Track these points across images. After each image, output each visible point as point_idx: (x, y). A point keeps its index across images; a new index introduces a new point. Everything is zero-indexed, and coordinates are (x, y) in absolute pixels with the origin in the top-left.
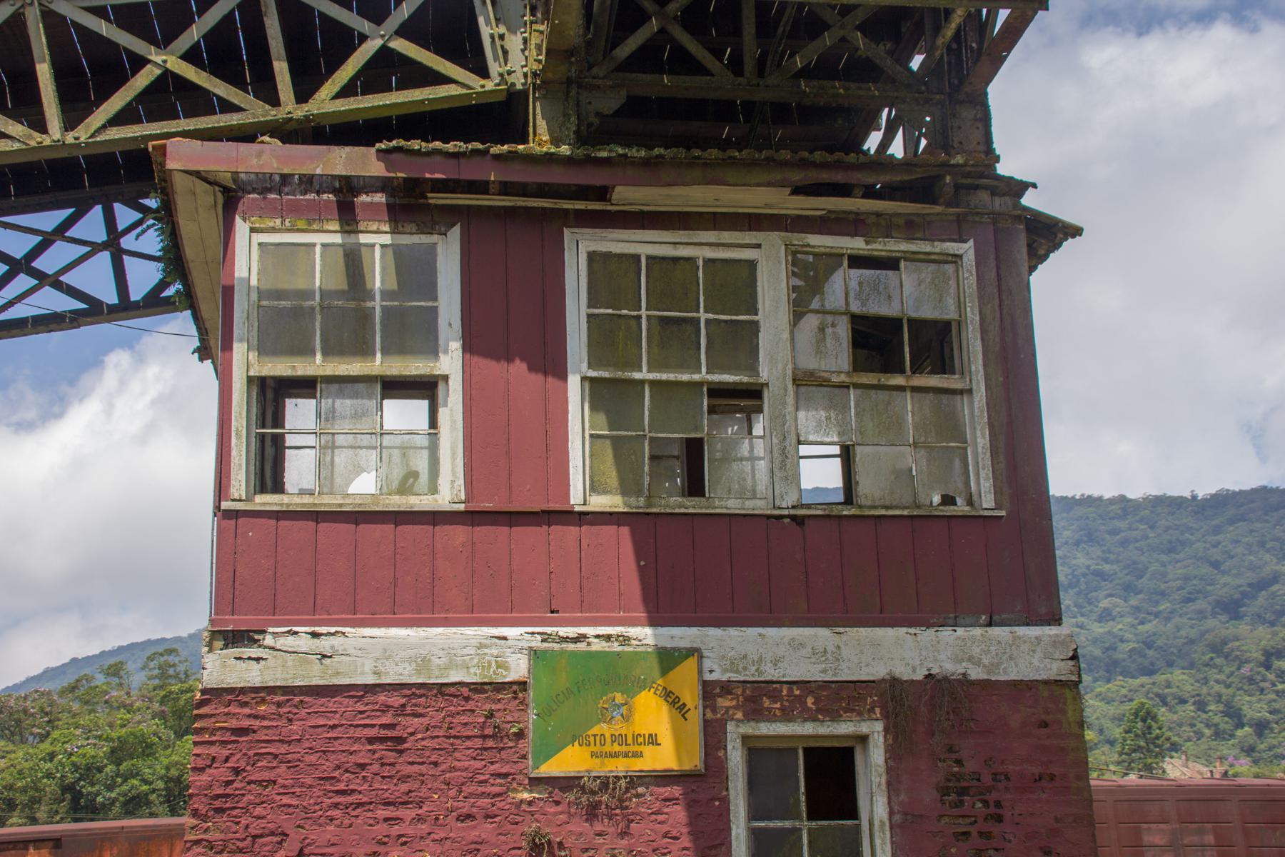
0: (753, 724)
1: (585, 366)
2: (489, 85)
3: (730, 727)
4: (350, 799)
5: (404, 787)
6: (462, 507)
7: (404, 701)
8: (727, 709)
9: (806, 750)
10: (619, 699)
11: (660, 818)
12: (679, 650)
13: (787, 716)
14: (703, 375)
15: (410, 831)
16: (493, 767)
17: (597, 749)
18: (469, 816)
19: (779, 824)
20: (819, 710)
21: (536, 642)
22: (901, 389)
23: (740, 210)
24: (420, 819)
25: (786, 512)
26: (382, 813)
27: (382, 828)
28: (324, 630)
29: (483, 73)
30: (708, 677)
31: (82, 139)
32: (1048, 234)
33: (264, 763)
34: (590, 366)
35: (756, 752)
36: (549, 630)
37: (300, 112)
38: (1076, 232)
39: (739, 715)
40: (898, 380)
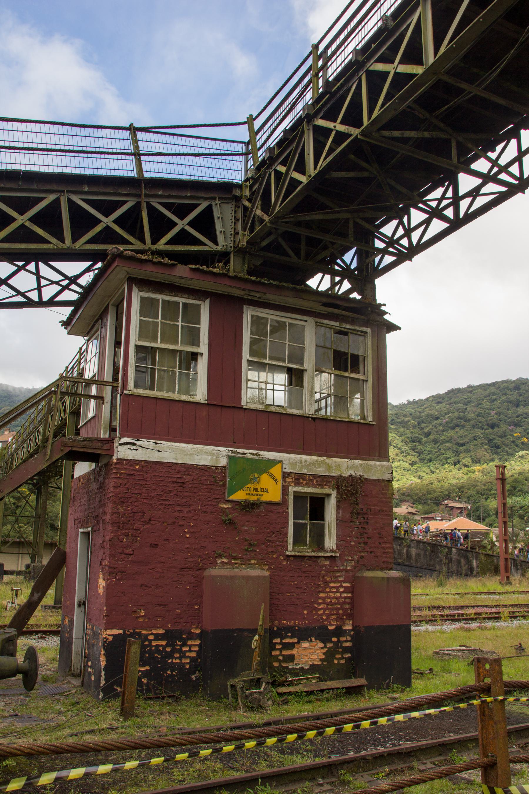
0: (297, 487)
1: (248, 356)
2: (219, 248)
3: (290, 488)
4: (167, 503)
5: (184, 500)
6: (206, 402)
7: (185, 470)
8: (289, 482)
9: (311, 498)
10: (256, 475)
11: (267, 517)
12: (276, 460)
13: (307, 485)
14: (179, 347)
15: (186, 516)
16: (214, 495)
17: (249, 492)
18: (206, 512)
19: (301, 521)
20: (318, 485)
21: (230, 453)
22: (346, 377)
23: (302, 308)
24: (189, 512)
25: (311, 416)
26: (177, 508)
27: (176, 514)
28: (159, 442)
29: (216, 243)
30: (284, 470)
31: (77, 248)
32: (392, 327)
33: (138, 487)
34: (250, 356)
35: (298, 497)
36: (234, 449)
37: (154, 248)
38: (399, 328)
39: (293, 484)
40: (346, 374)
